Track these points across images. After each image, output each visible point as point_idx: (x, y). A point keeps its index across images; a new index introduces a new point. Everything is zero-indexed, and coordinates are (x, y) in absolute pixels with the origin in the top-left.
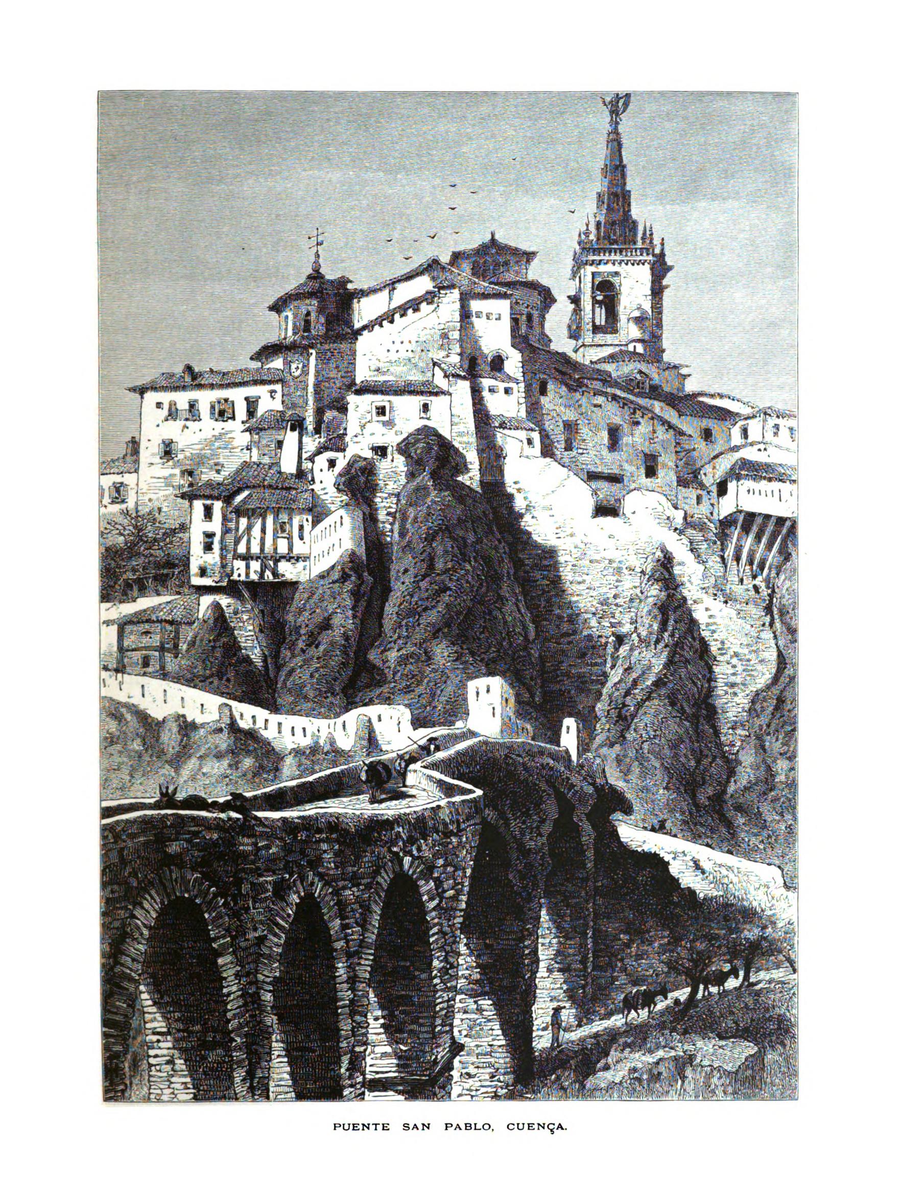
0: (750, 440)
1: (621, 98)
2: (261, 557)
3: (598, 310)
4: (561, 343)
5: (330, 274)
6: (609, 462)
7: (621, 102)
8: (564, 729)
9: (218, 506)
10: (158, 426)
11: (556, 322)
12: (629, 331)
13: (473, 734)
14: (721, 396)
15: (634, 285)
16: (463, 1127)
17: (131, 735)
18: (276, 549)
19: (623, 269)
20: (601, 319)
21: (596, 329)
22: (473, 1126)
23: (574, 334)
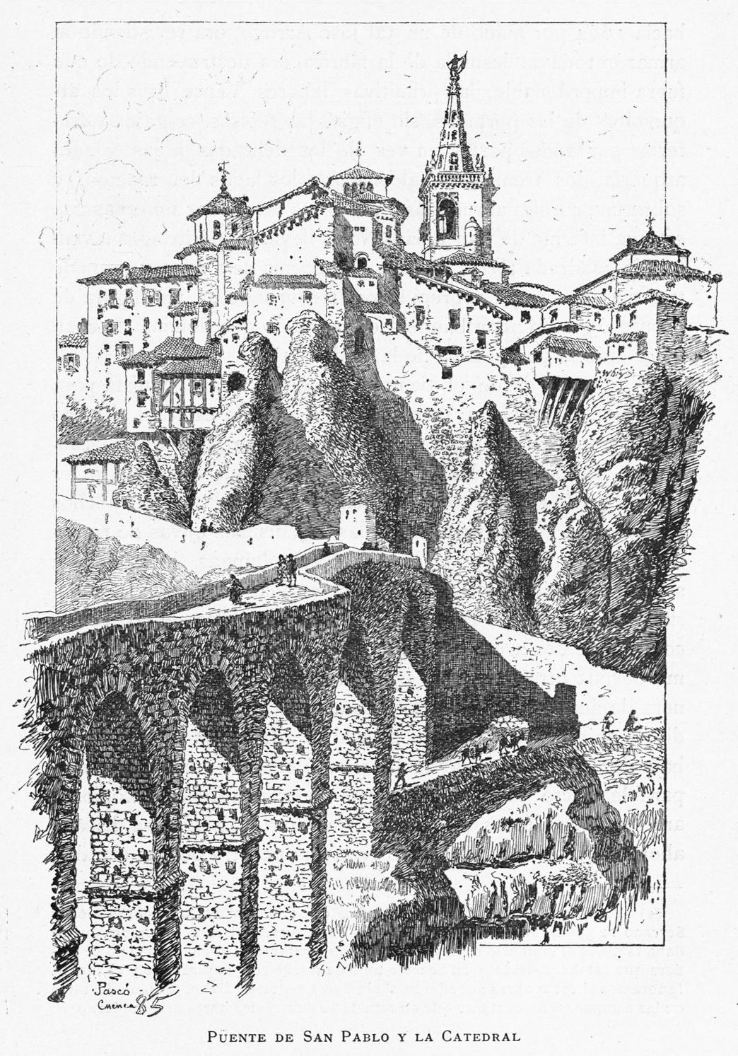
0: (611, 729)
1: (459, 59)
2: (182, 410)
3: (441, 222)
4: (414, 245)
5: (235, 192)
6: (451, 338)
7: (460, 63)
8: (414, 545)
9: (148, 372)
10: (133, 524)
11: (410, 230)
12: (465, 237)
13: (345, 547)
14: (530, 285)
15: (468, 202)
16: (362, 1038)
17: (76, 546)
18: (192, 403)
19: (460, 190)
20: (443, 227)
21: (440, 236)
22: (371, 1037)
23: (424, 237)
